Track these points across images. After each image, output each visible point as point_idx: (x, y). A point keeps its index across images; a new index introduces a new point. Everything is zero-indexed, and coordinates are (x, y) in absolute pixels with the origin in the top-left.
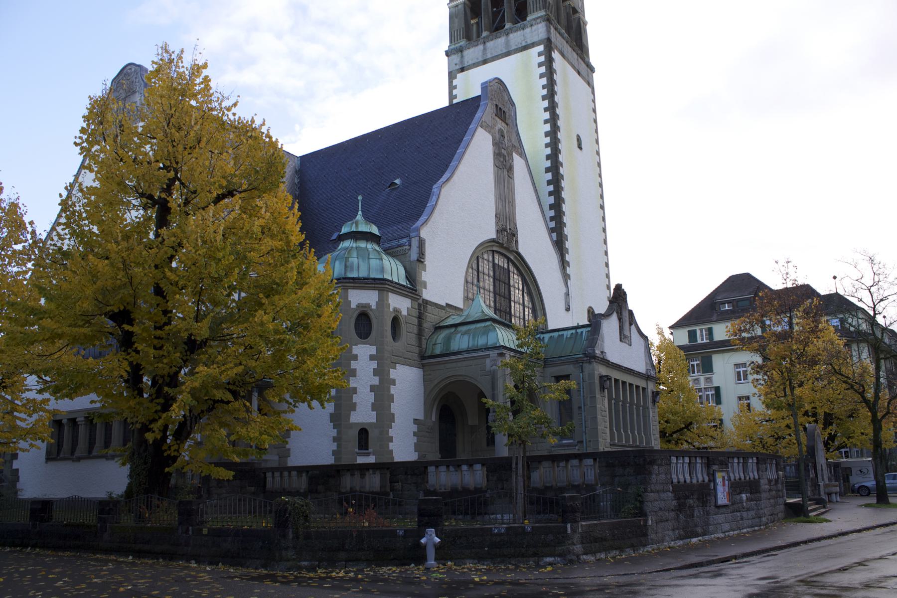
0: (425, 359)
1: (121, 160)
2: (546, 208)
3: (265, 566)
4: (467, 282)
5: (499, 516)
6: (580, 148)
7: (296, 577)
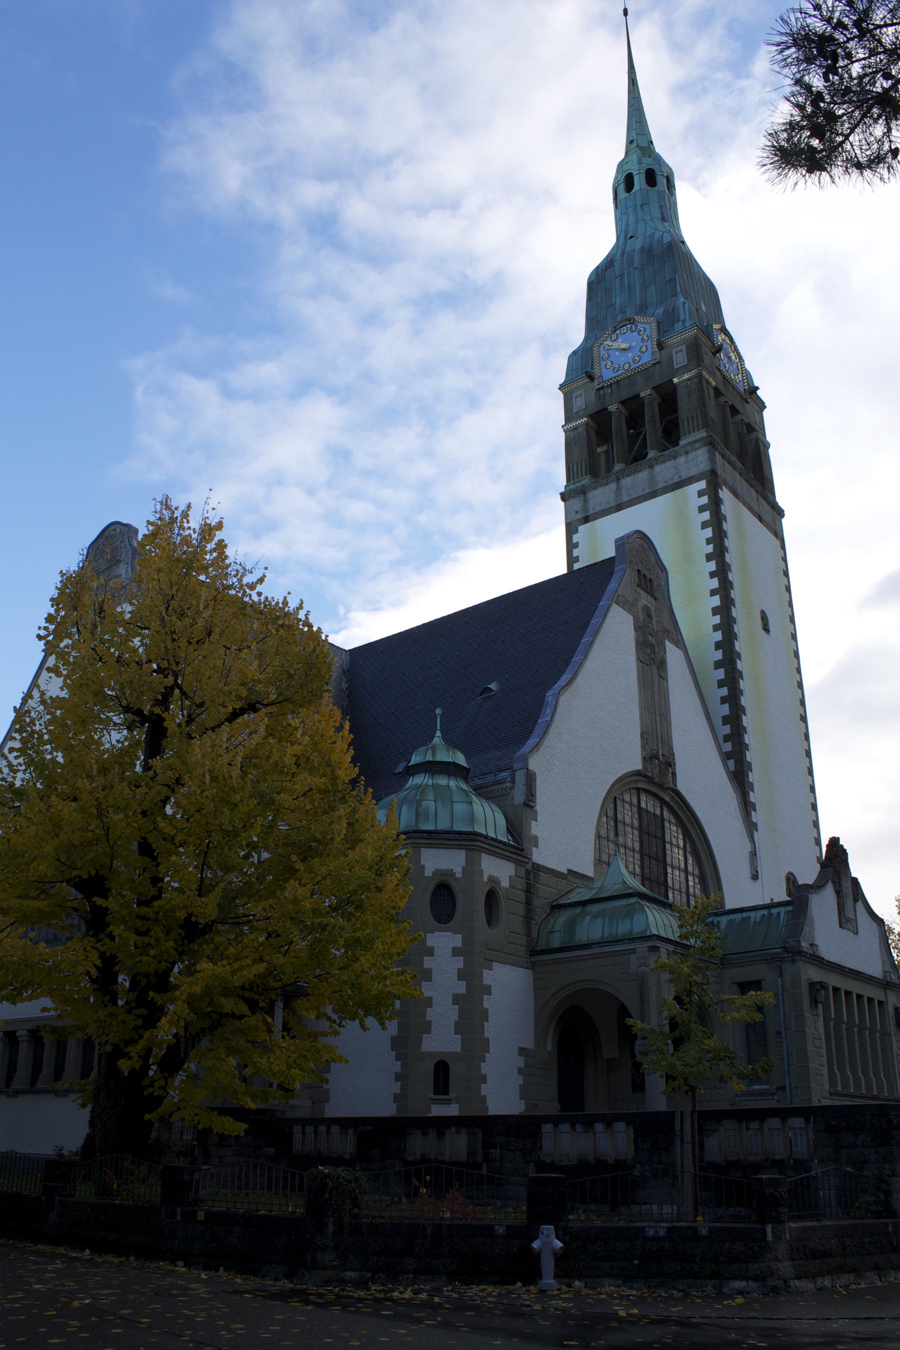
0: (536, 955)
1: (100, 660)
2: (718, 722)
3: (289, 1276)
4: (599, 836)
5: (655, 1207)
6: (766, 629)
7: (338, 1296)
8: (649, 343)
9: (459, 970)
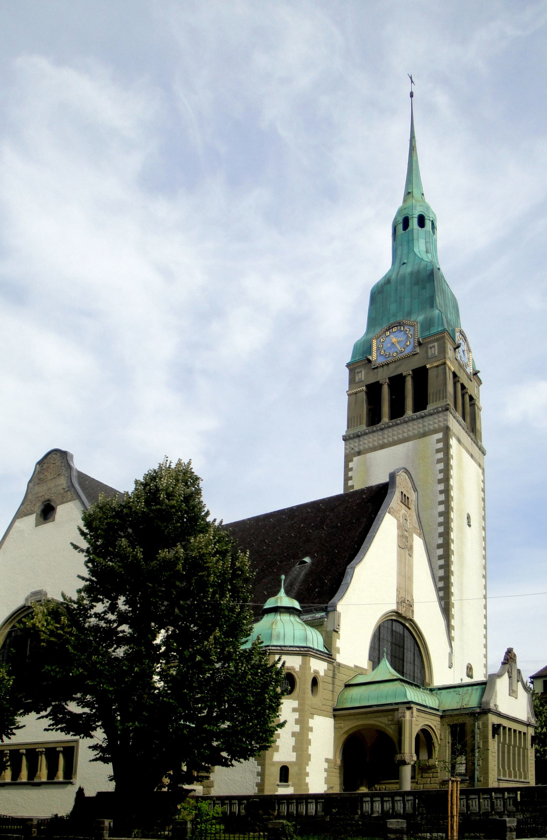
8: (412, 340)
9: (296, 719)
